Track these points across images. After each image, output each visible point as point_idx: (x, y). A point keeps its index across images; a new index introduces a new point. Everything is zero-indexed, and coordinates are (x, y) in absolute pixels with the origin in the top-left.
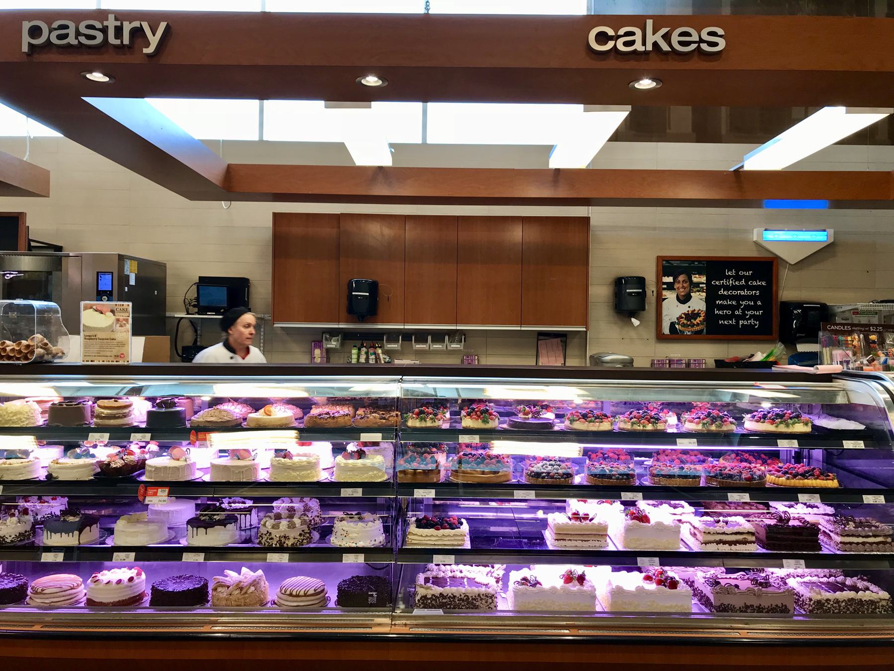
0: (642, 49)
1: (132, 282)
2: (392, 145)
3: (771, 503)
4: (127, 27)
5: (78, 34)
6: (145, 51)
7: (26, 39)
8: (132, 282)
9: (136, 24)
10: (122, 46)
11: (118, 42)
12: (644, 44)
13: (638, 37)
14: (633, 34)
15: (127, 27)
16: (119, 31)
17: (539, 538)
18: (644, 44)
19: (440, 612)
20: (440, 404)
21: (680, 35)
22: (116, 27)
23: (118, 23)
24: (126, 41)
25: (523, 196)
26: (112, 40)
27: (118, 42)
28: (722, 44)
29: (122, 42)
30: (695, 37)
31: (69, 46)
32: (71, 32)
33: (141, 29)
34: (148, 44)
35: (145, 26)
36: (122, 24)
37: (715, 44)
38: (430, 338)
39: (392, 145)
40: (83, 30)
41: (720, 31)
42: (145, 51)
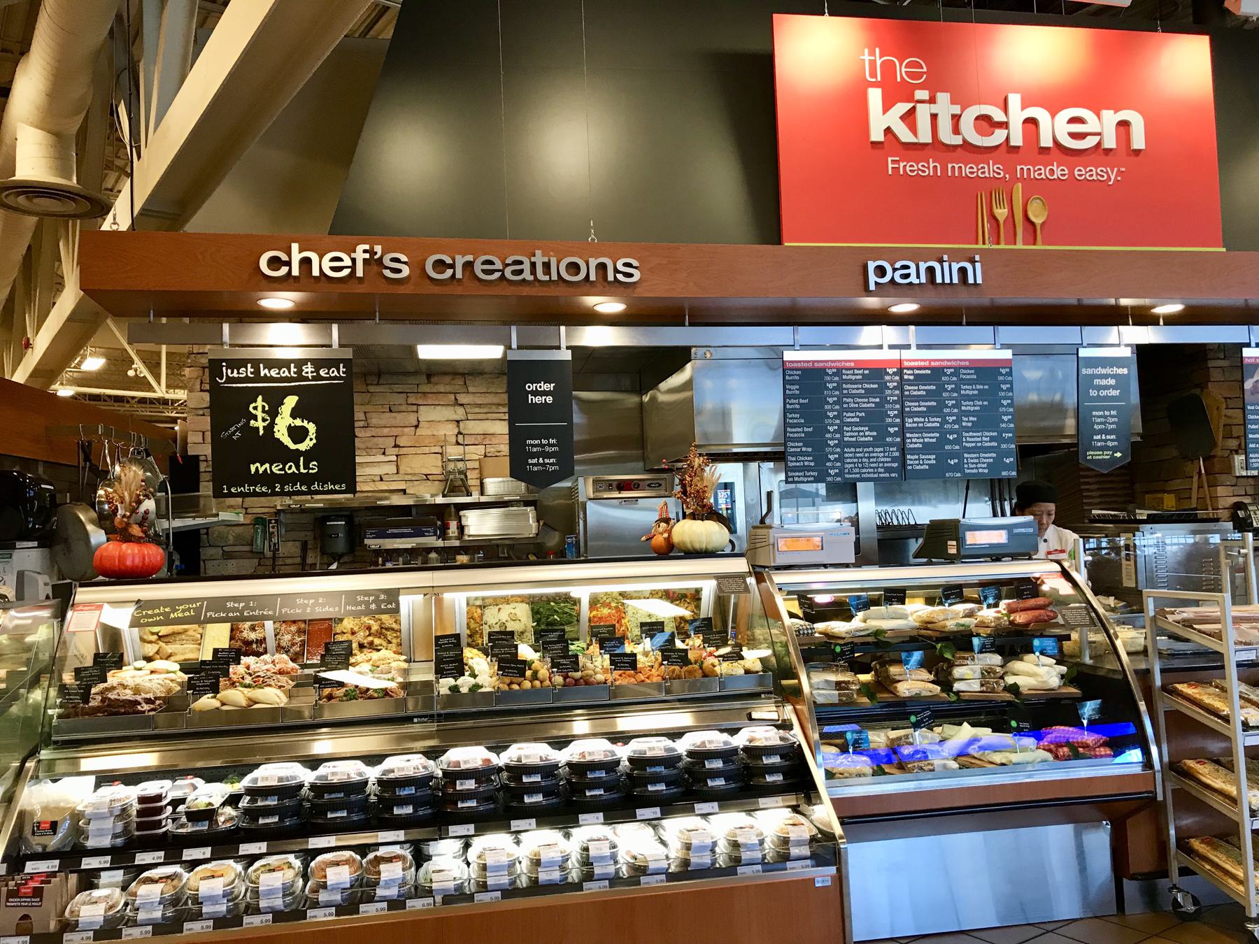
0: (917, 281)
5: (616, 271)
10: (920, 284)
11: (547, 278)
12: (918, 277)
13: (913, 271)
14: (908, 267)
18: (918, 277)
19: (427, 352)
20: (805, 347)
21: (483, 263)
23: (546, 260)
27: (547, 278)
28: (406, 271)
30: (499, 265)
31: (911, 284)
32: (526, 267)
37: (631, 275)
40: (620, 267)
41: (404, 258)
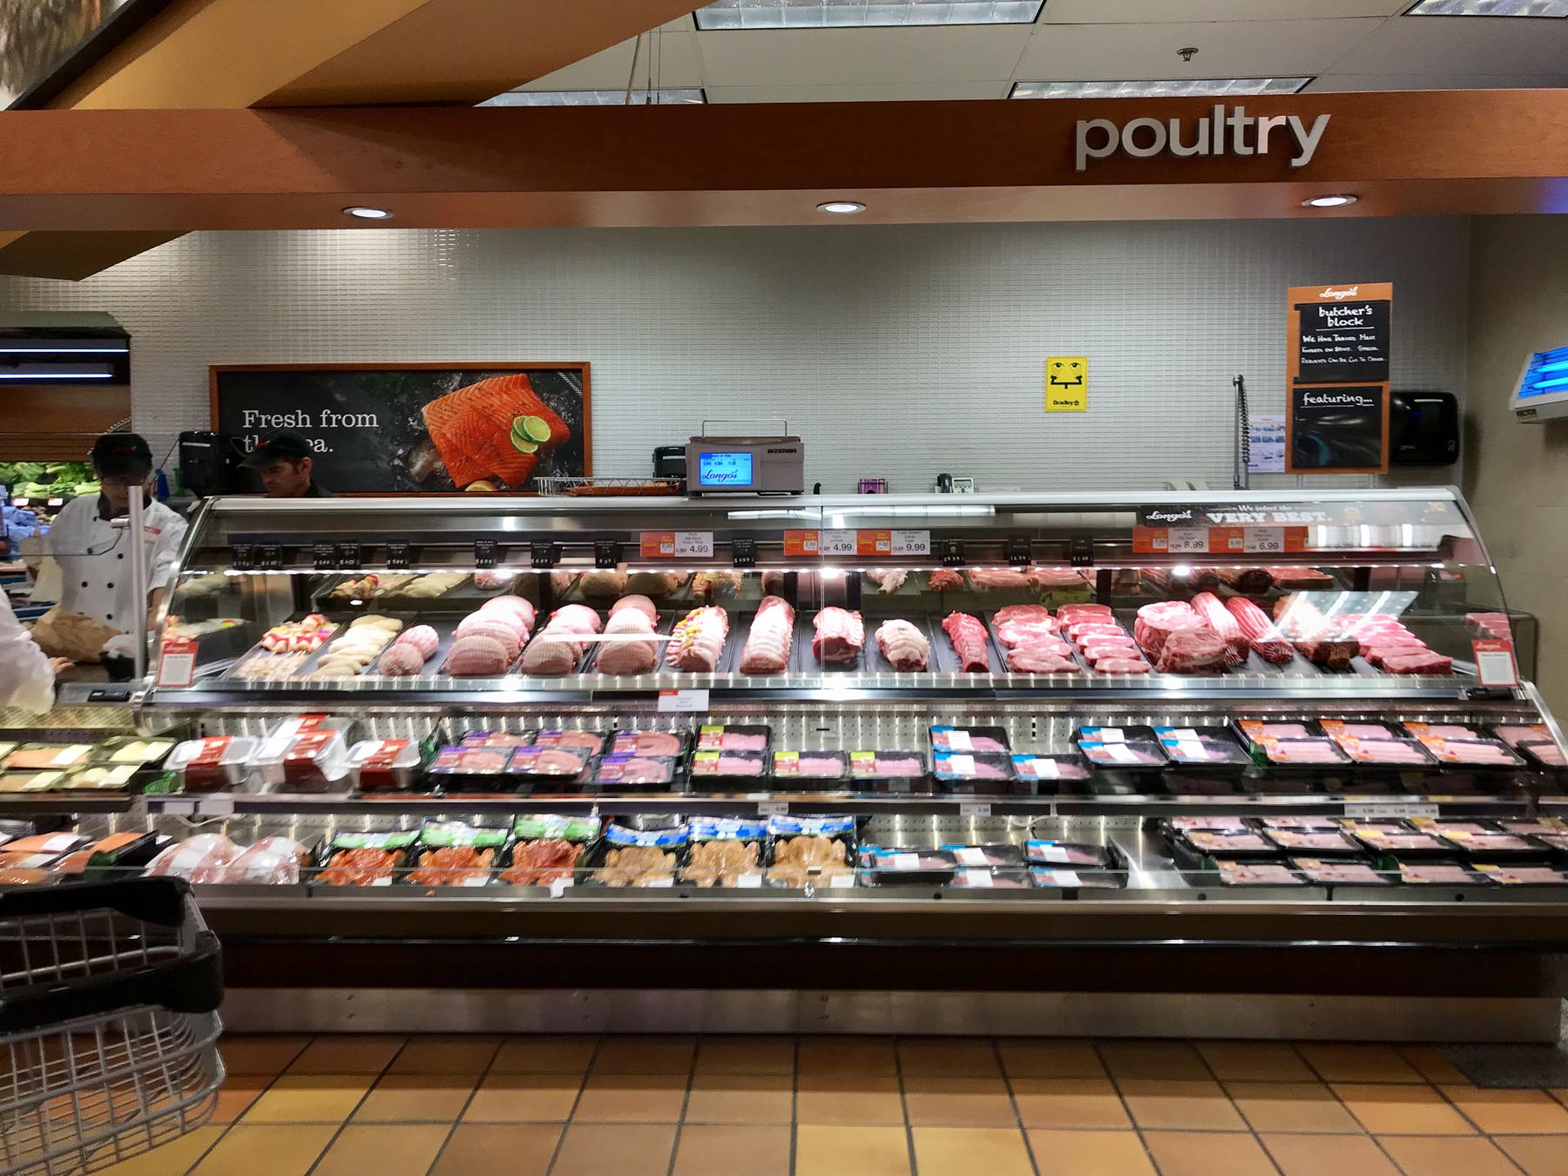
1: (1382, 291)
2: (1297, 307)
3: (1267, 821)
4: (1265, 125)
6: (1296, 162)
7: (1083, 150)
8: (1382, 291)
9: (1280, 120)
15: (1265, 125)
16: (1251, 135)
17: (1247, 482)
22: (1246, 127)
23: (1250, 121)
24: (1263, 148)
25: (1423, 1000)
26: (1240, 148)
29: (1256, 150)
33: (1288, 127)
34: (1298, 152)
35: (1296, 122)
36: (1256, 123)
38: (59, 977)
39: (1297, 307)
42: (1296, 162)
